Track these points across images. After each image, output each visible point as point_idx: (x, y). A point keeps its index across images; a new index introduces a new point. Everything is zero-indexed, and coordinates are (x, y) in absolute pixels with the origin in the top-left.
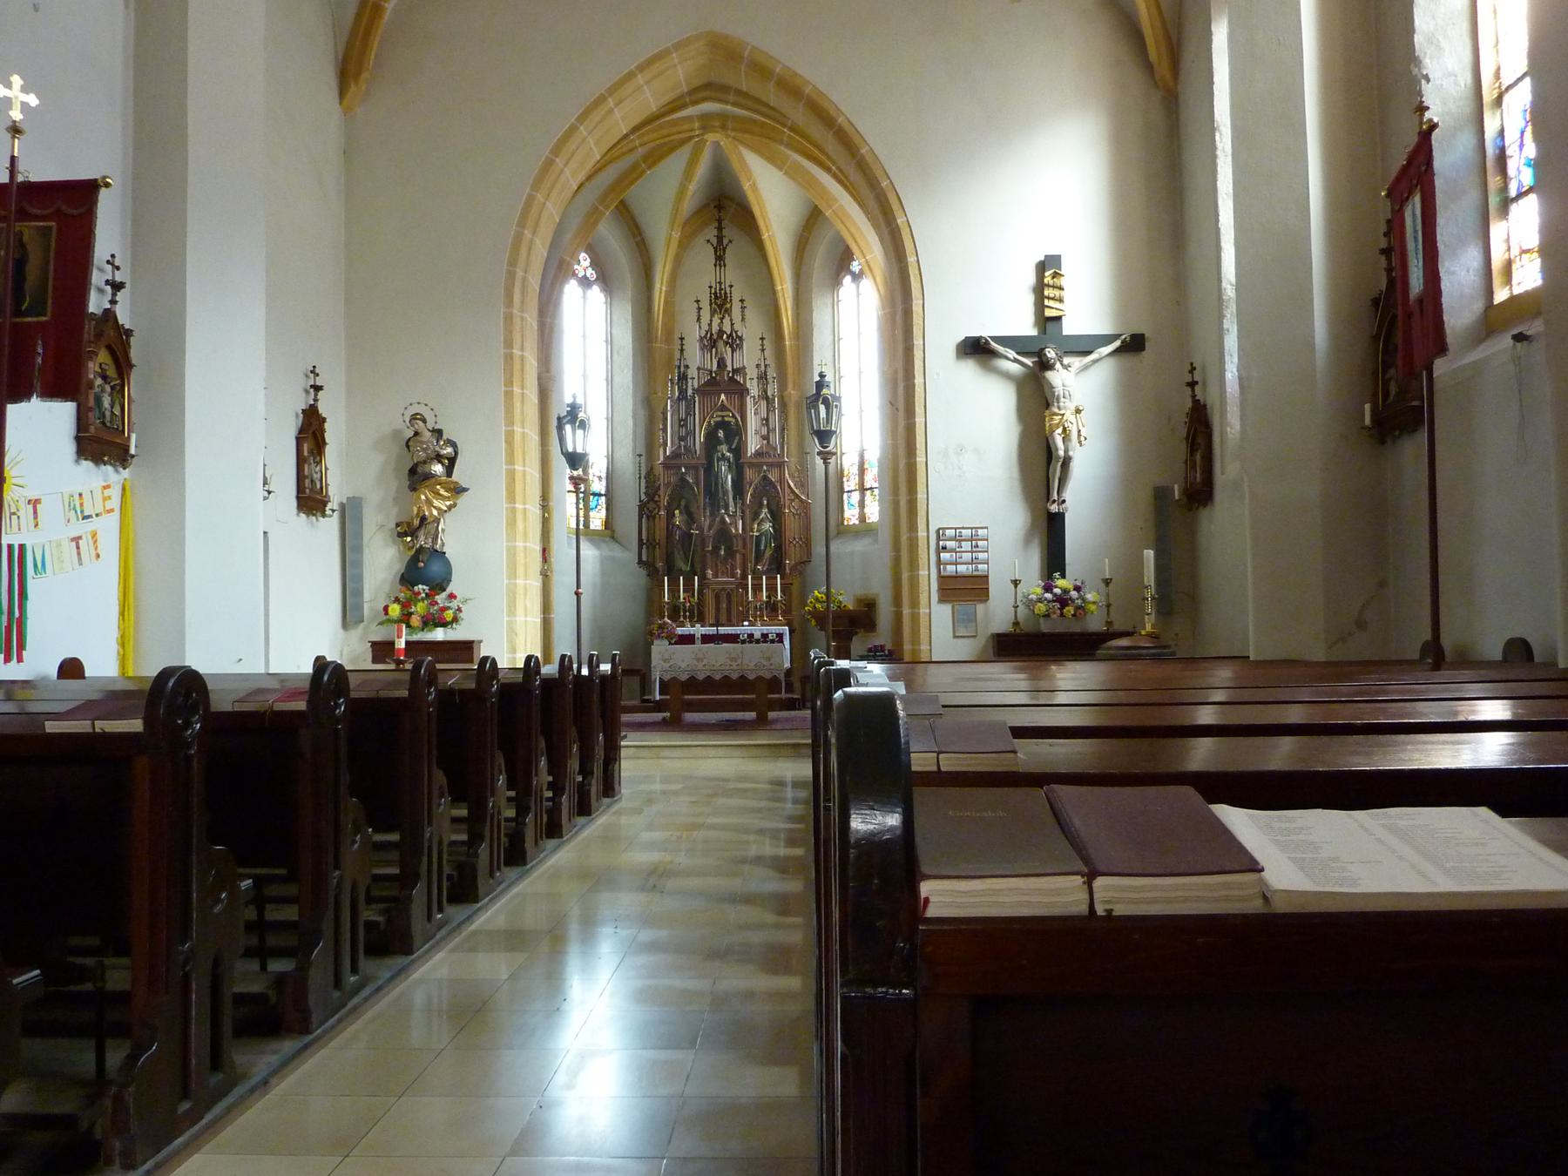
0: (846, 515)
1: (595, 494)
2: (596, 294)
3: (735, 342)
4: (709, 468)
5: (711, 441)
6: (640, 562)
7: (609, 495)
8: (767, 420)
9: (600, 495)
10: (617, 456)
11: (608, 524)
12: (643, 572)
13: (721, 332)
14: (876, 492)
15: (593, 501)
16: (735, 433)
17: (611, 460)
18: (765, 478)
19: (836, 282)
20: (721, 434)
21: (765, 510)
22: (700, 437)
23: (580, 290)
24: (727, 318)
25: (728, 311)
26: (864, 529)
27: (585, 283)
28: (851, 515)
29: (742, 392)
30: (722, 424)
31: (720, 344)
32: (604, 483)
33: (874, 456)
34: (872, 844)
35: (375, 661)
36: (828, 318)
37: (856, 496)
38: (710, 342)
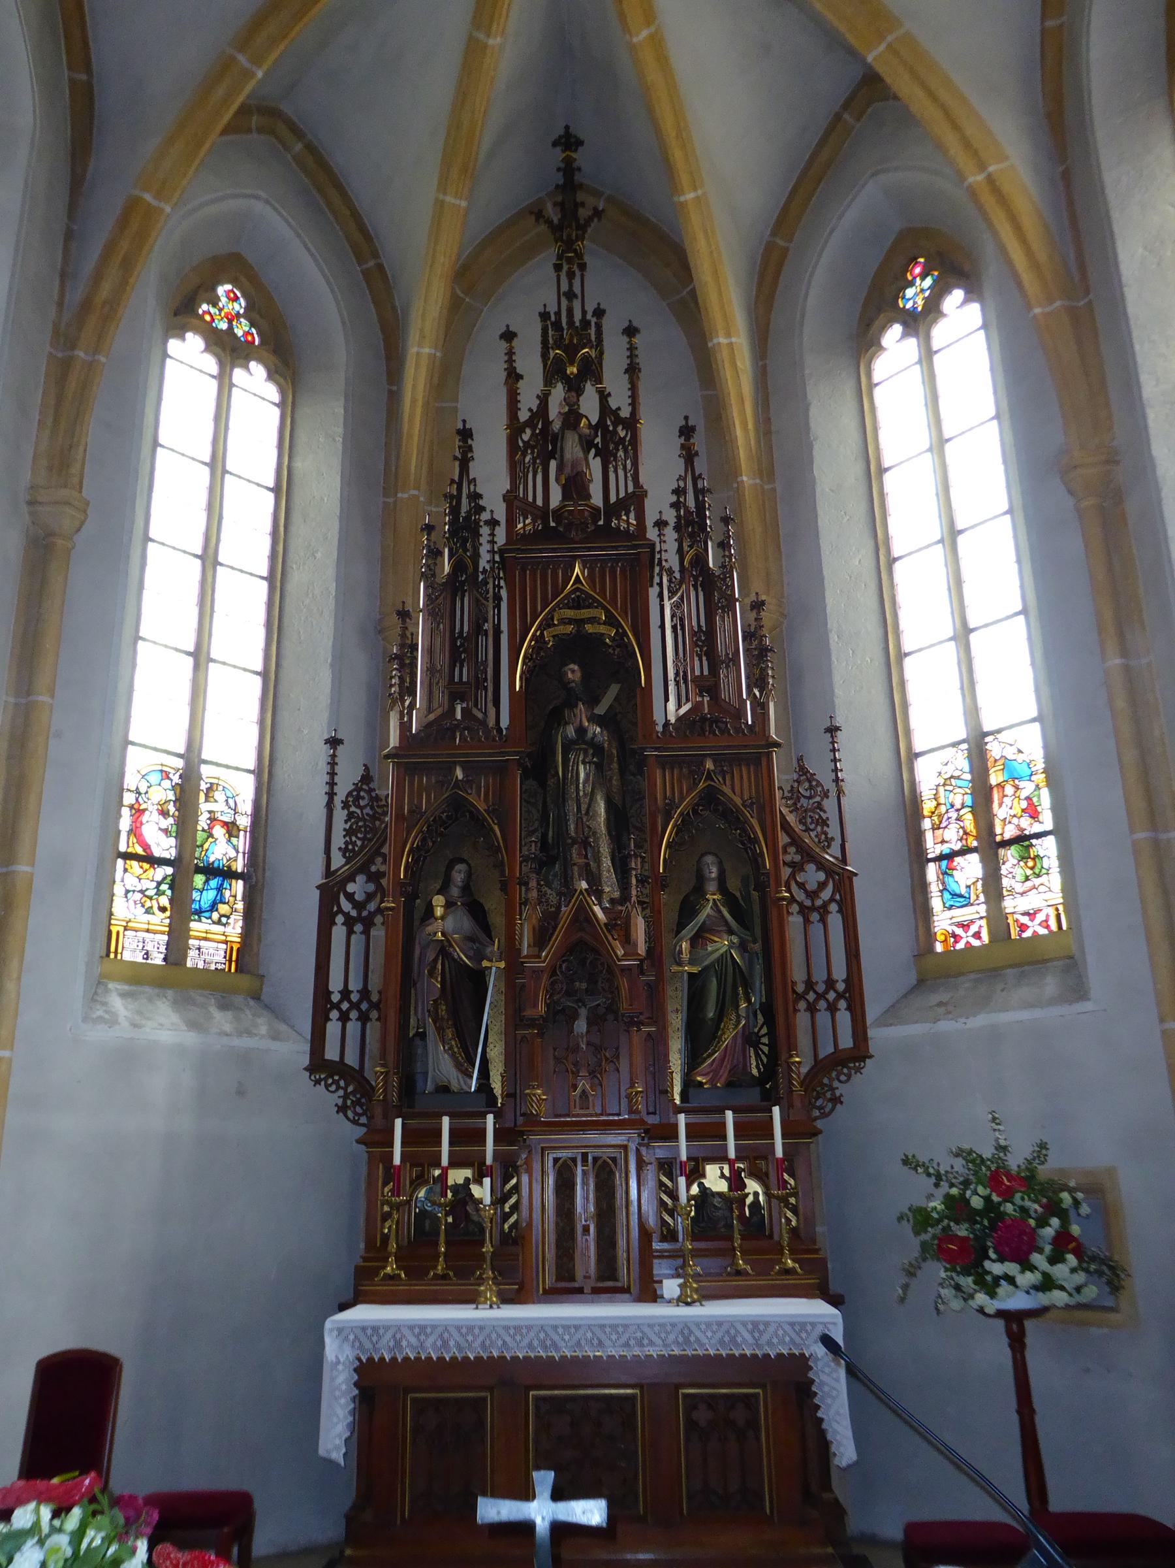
0: (943, 921)
1: (210, 871)
2: (255, 383)
3: (616, 437)
4: (539, 767)
5: (544, 703)
6: (319, 1066)
7: (256, 877)
8: (710, 633)
9: (227, 874)
10: (283, 772)
11: (246, 956)
12: (327, 1098)
13: (572, 418)
14: (1048, 848)
15: (203, 892)
16: (614, 666)
17: (266, 775)
18: (711, 798)
19: (865, 344)
20: (573, 673)
21: (713, 896)
22: (513, 677)
23: (210, 363)
24: (590, 391)
25: (592, 370)
26: (1009, 960)
27: (229, 351)
28: (956, 921)
29: (640, 563)
30: (580, 646)
31: (572, 448)
32: (242, 842)
33: (1023, 744)
34: (464, 770)
35: (762, 1100)
36: (849, 422)
37: (970, 869)
38: (534, 441)
